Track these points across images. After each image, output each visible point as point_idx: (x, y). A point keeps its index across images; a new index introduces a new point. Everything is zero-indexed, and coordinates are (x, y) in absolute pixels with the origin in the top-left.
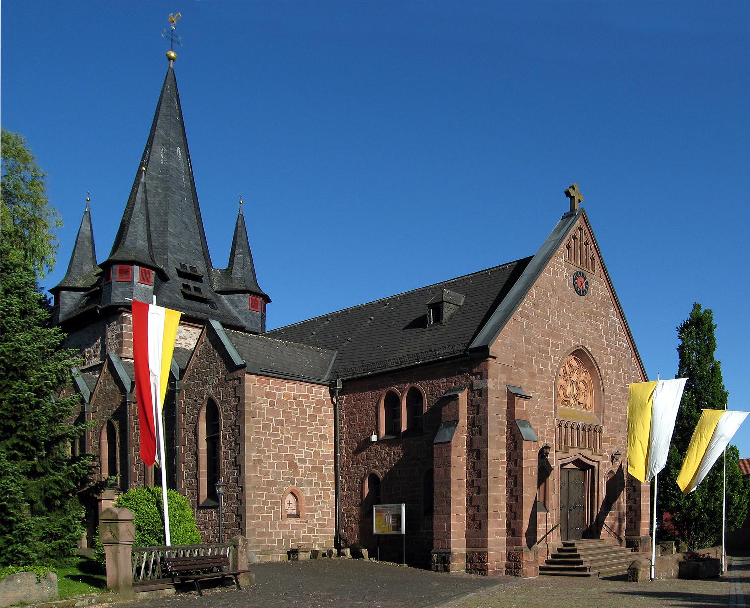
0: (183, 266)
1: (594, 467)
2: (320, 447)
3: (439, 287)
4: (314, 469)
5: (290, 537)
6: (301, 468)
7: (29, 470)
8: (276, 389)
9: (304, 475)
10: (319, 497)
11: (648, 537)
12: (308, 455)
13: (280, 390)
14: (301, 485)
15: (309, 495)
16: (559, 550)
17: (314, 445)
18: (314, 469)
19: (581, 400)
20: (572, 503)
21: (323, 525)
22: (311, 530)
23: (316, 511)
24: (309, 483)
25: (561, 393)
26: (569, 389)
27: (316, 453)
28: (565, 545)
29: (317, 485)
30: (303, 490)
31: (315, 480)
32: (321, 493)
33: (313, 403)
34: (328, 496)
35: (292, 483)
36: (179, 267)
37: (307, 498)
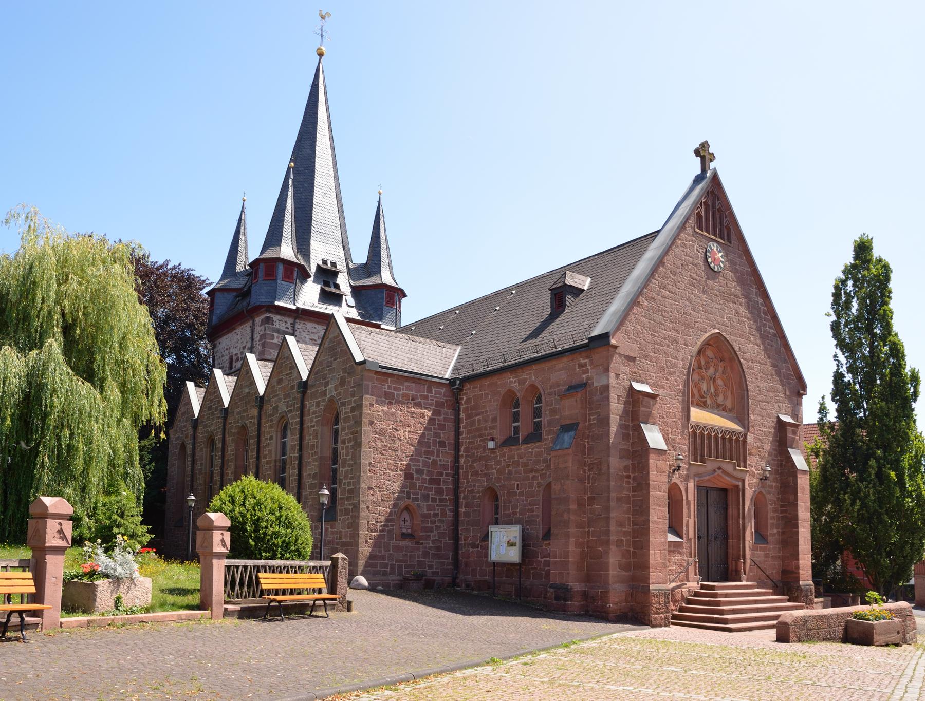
0: (325, 262)
1: (738, 486)
2: (438, 456)
3: (562, 272)
4: (432, 481)
5: (405, 561)
6: (418, 479)
7: (769, 469)
8: (395, 389)
9: (420, 488)
10: (436, 515)
11: (810, 585)
12: (426, 464)
13: (399, 389)
14: (416, 499)
15: (425, 512)
16: (696, 594)
17: (432, 453)
18: (432, 481)
19: (720, 399)
20: (712, 532)
21: (438, 548)
22: (426, 554)
23: (432, 531)
24: (426, 498)
25: (695, 391)
26: (704, 387)
27: (435, 462)
28: (703, 587)
29: (434, 500)
30: (418, 506)
31: (432, 494)
32: (438, 510)
33: (432, 405)
34: (444, 514)
35: (408, 497)
36: (320, 263)
37: (424, 516)
